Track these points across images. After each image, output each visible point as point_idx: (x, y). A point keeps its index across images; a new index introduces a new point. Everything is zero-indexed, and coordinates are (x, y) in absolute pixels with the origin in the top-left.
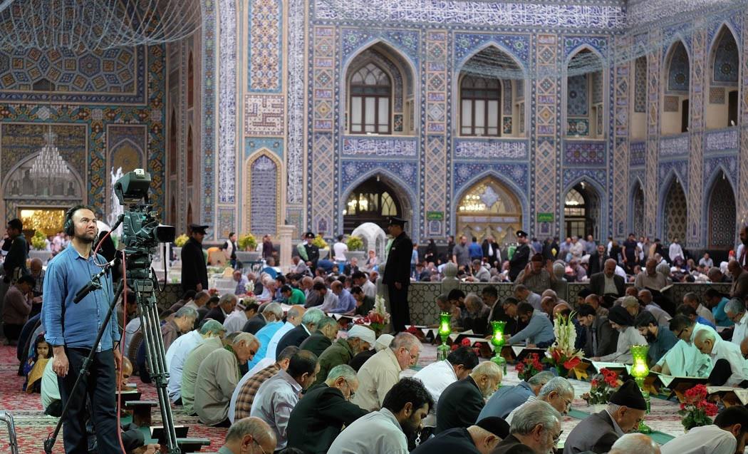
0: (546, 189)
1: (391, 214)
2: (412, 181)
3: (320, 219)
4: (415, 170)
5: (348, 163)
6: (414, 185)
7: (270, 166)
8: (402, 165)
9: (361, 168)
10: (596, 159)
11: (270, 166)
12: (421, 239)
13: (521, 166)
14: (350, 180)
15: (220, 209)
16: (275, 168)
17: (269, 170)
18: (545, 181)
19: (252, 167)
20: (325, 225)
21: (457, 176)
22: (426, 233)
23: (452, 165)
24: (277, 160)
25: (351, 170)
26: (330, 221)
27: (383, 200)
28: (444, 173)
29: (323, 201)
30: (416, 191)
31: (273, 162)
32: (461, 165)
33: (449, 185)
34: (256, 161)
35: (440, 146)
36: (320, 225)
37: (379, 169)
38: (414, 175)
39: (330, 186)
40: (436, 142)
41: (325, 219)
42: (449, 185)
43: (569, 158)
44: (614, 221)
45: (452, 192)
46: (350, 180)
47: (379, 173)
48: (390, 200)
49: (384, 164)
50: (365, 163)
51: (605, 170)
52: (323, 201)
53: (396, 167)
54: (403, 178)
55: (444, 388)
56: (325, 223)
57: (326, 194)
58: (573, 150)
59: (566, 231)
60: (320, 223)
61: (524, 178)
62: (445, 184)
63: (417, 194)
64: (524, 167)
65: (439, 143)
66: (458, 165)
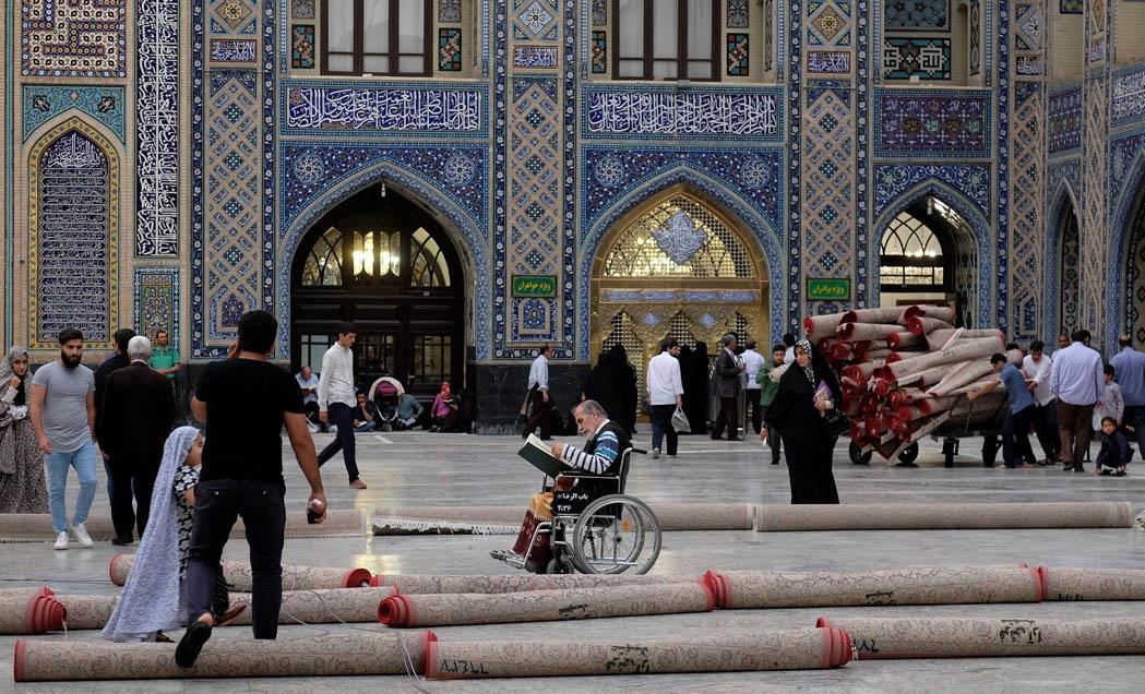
0: (829, 214)
8: (446, 153)
9: (337, 161)
25: (309, 169)
37: (385, 165)
38: (477, 182)
40: (829, 100)
42: (570, 207)
49: (397, 154)
50: (347, 150)
57: (242, 232)
61: (477, 182)
64: (771, 158)
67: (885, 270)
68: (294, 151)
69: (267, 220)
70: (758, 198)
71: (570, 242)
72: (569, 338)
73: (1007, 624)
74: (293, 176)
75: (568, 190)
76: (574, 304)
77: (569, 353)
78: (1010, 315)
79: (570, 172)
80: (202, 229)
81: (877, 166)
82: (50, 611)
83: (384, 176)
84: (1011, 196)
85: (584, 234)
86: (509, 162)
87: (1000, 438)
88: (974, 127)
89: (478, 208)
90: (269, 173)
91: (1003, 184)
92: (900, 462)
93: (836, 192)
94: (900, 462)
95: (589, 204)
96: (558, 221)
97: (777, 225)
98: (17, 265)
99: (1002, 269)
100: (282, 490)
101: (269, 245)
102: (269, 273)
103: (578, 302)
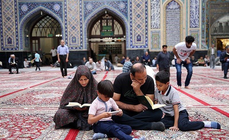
1: (120, 34)
2: (59, 13)
3: (137, 35)
6: (126, 14)
7: (177, 6)
11: (177, 6)
14: (24, 14)
15: (152, 32)
16: (180, 8)
17: (176, 9)
19: (167, 8)
21: (21, 11)
24: (181, 3)
25: (25, 8)
26: (143, 35)
27: (115, 26)
30: (127, 18)
31: (178, 4)
33: (16, 17)
34: (168, 4)
37: (41, 7)
38: (126, 8)
41: (140, 35)
42: (16, 17)
44: (133, 34)
46: (24, 14)
48: (119, 25)
54: (120, 10)
55: (176, 79)
59: (95, 41)
61: (126, 8)
63: (128, 21)
67: (109, 25)
69: (16, 21)
70: (57, 13)
72: (81, 44)
73: (205, 96)
74: (21, 10)
75: (16, 13)
76: (18, 38)
77: (82, 48)
78: (133, 38)
80: (2, 23)
82: (74, 132)
84: (133, 11)
85: (20, 23)
86: (2, 8)
87: (138, 58)
89: (126, 14)
90: (16, 11)
91: (131, 9)
93: (10, 14)
94: (222, 41)
95: (20, 15)
96: (14, 21)
97: (127, 18)
98: (185, 28)
99: (146, 24)
100: (189, 83)
101: (17, 26)
103: (19, 37)
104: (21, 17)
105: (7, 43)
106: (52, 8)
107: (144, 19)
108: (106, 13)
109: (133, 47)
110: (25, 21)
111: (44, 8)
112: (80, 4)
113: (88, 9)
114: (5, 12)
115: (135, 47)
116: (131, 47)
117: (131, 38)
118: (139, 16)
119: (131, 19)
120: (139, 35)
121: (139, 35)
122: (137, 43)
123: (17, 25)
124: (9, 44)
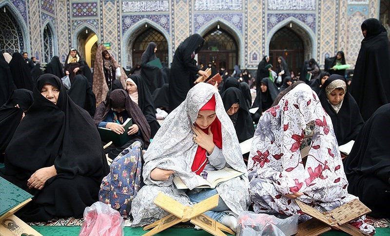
0: (255, 31)
1: (233, 49)
4: (241, 19)
5: (126, 17)
6: (314, 29)
8: (232, 15)
9: (280, 17)
10: (92, 12)
12: (246, 65)
13: (312, 15)
18: (254, 26)
20: (256, 56)
22: (248, 61)
23: (71, 21)
25: (274, 19)
28: (116, 23)
29: (255, 41)
32: (126, 17)
35: (112, 6)
36: (253, 57)
39: (115, 33)
40: (110, 4)
41: (256, 53)
42: (264, 30)
43: (75, 13)
45: (266, 35)
47: (291, 22)
49: (148, 17)
50: (282, 14)
51: (98, 20)
52: (255, 41)
53: (302, 17)
56: (256, 55)
57: (257, 37)
58: (77, 8)
60: (253, 55)
61: (314, 23)
62: (116, 31)
64: (166, 16)
65: (112, 4)
66: (124, 17)
68: (124, 17)
71: (264, 39)
78: (249, 56)
79: (264, 22)
81: (73, 21)
83: (146, 23)
84: (104, 28)
88: (95, 10)
89: (314, 29)
92: (68, 63)
94: (68, 63)
102: (264, 47)
104: (269, 29)
105: (252, 59)
106: (230, 20)
107: (117, 36)
108: (219, 28)
109: (248, 67)
110: (132, 35)
111: (222, 20)
112: (263, 17)
113: (126, 24)
114: (107, 25)
115: (251, 66)
116: (246, 66)
117: (246, 56)
118: (110, 33)
119: (319, 35)
120: (255, 53)
121: (255, 53)
122: (252, 62)
123: (264, 39)
124: (254, 61)
